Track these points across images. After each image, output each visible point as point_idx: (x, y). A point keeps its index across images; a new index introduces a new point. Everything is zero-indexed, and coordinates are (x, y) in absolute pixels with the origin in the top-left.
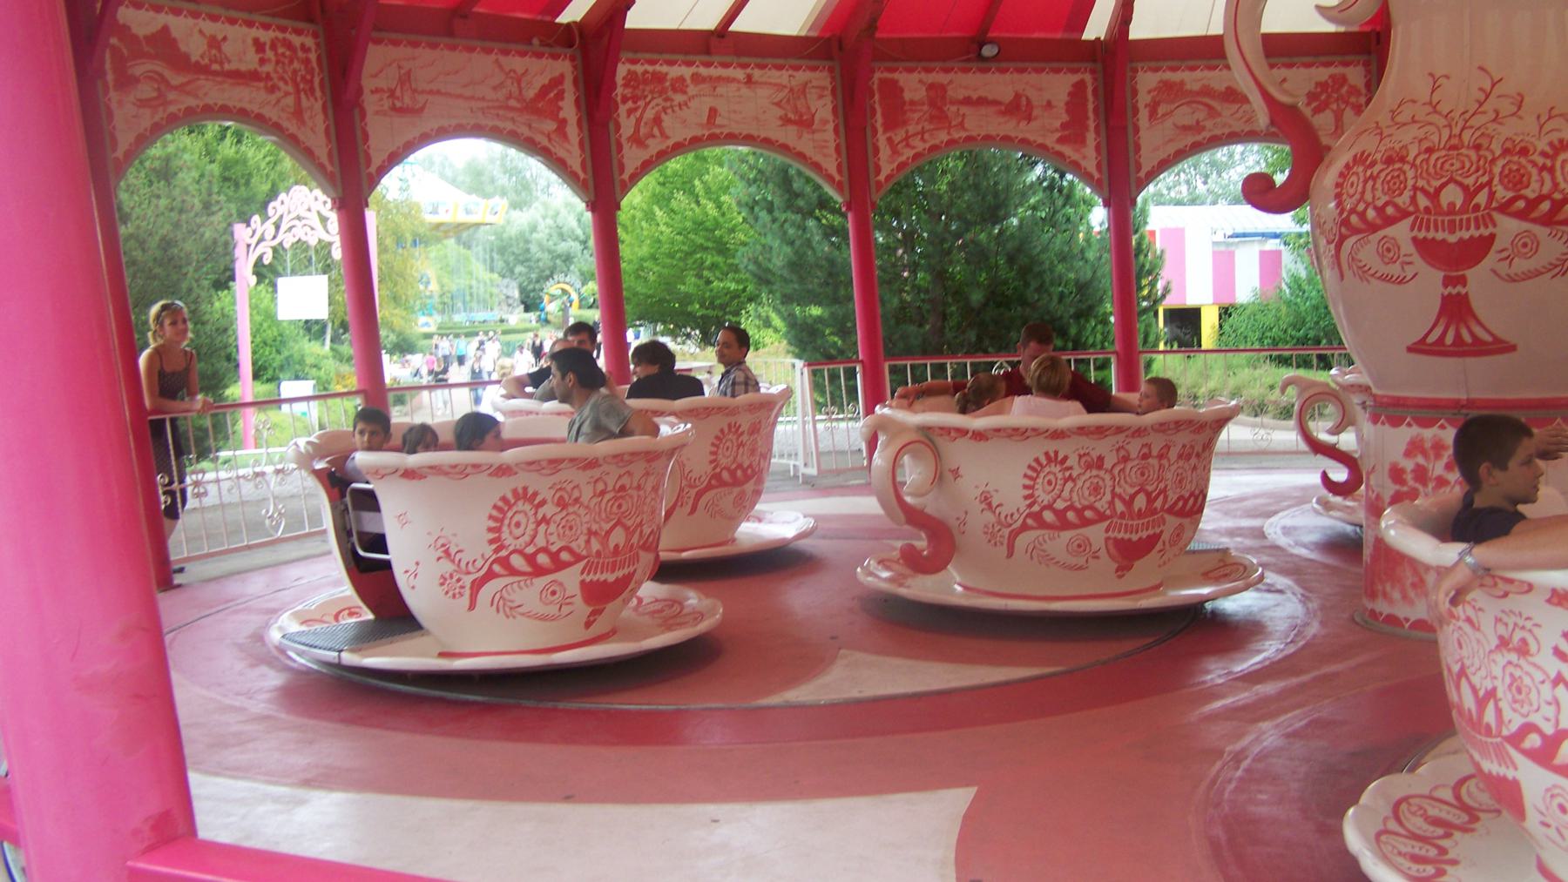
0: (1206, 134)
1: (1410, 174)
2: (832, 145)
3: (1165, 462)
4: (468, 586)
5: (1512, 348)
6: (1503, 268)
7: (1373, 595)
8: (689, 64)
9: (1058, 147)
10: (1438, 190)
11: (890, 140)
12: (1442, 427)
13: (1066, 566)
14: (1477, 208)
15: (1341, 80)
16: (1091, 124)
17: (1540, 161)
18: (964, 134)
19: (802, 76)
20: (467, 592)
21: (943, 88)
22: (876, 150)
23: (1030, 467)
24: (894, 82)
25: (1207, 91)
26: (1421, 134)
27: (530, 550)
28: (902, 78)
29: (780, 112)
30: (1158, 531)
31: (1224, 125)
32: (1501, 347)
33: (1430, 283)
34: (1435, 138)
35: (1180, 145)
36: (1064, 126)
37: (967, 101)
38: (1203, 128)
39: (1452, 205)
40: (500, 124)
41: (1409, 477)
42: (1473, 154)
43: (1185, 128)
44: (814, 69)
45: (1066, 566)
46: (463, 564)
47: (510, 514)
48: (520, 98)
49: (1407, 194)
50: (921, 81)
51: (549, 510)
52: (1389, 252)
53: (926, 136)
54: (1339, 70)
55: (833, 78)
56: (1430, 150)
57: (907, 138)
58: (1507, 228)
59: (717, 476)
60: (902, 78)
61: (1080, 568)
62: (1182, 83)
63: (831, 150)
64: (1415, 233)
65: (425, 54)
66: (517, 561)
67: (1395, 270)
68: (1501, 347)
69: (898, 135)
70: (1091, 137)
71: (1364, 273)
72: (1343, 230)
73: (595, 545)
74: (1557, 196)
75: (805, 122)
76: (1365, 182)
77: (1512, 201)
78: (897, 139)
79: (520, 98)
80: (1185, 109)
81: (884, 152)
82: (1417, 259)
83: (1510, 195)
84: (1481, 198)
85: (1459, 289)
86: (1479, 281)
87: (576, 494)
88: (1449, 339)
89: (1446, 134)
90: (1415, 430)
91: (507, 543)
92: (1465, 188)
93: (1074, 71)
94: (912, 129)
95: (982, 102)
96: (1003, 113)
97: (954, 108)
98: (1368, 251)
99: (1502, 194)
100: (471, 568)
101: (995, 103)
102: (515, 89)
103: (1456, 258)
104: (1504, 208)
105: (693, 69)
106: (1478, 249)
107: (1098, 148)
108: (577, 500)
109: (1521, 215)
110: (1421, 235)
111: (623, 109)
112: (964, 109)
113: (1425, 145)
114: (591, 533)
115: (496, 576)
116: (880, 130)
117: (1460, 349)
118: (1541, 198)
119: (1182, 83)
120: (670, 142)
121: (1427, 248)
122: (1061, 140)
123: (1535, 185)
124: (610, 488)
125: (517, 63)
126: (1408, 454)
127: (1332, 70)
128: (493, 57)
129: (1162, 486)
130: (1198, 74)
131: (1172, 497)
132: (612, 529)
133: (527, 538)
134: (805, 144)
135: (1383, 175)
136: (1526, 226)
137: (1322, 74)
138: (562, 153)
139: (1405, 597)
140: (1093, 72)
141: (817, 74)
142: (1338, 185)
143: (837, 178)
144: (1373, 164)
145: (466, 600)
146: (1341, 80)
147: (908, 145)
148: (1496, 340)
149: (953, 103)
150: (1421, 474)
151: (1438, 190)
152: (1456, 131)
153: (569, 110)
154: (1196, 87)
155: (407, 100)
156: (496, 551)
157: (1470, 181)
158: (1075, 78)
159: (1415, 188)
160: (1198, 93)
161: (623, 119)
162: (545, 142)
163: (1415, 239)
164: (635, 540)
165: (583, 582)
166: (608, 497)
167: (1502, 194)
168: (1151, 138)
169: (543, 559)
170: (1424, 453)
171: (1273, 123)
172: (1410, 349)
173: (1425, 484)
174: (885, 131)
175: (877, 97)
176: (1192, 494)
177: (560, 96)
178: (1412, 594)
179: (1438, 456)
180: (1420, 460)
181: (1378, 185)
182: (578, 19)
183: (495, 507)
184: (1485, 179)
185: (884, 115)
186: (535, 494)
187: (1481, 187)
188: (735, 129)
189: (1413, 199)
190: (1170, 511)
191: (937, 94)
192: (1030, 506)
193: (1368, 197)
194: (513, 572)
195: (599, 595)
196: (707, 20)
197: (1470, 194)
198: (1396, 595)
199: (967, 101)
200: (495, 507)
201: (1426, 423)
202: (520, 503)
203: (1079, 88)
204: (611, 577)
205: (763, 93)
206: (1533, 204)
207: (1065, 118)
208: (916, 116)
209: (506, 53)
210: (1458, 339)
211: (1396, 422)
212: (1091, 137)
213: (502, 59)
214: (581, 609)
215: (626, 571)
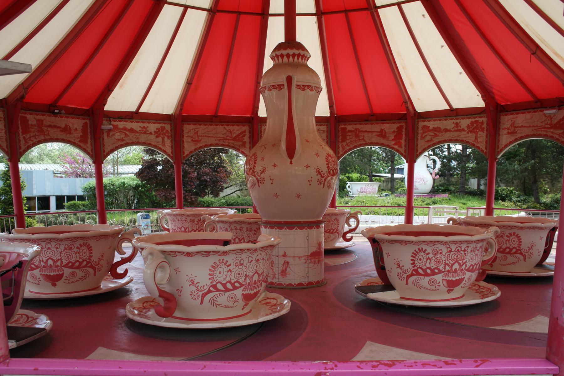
0: (125, 142)
2: (4, 138)
3: (466, 252)
4: (201, 295)
9: (79, 144)
11: (24, 138)
13: (225, 307)
15: (163, 128)
16: (89, 137)
18: (49, 137)
21: (42, 121)
22: (20, 141)
23: (413, 253)
24: (26, 118)
25: (125, 129)
27: (224, 282)
28: (28, 116)
30: (463, 277)
31: (130, 139)
35: (117, 145)
36: (81, 137)
37: (50, 126)
38: (124, 140)
40: (542, 133)
43: (119, 140)
46: (199, 288)
50: (34, 118)
51: (431, 256)
53: (37, 137)
54: (164, 125)
55: (4, 114)
57: (30, 138)
60: (28, 116)
61: (231, 307)
62: (117, 125)
63: (4, 140)
69: (28, 136)
70: (89, 141)
78: (27, 138)
80: (118, 134)
81: (22, 142)
87: (242, 262)
93: (84, 119)
94: (32, 134)
95: (55, 127)
96: (61, 131)
97: (46, 128)
101: (59, 127)
107: (91, 145)
108: (242, 264)
112: (49, 129)
114: (446, 264)
115: (211, 292)
116: (21, 134)
119: (117, 125)
122: (80, 141)
127: (161, 125)
129: (464, 261)
130: (122, 123)
131: (468, 265)
132: (254, 274)
137: (158, 126)
140: (89, 119)
143: (6, 150)
145: (199, 301)
146: (163, 128)
147: (30, 140)
149: (45, 126)
154: (122, 127)
155: (196, 138)
158: (85, 121)
160: (122, 129)
162: (557, 137)
164: (261, 279)
165: (243, 294)
168: (108, 142)
174: (23, 134)
175: (19, 122)
176: (475, 264)
185: (22, 129)
190: (468, 270)
191: (40, 123)
192: (414, 267)
194: (218, 290)
195: (248, 298)
196: (134, 109)
199: (50, 126)
202: (221, 265)
203: (85, 124)
204: (252, 292)
207: (81, 134)
208: (33, 130)
212: (89, 141)
214: (241, 303)
215: (257, 290)
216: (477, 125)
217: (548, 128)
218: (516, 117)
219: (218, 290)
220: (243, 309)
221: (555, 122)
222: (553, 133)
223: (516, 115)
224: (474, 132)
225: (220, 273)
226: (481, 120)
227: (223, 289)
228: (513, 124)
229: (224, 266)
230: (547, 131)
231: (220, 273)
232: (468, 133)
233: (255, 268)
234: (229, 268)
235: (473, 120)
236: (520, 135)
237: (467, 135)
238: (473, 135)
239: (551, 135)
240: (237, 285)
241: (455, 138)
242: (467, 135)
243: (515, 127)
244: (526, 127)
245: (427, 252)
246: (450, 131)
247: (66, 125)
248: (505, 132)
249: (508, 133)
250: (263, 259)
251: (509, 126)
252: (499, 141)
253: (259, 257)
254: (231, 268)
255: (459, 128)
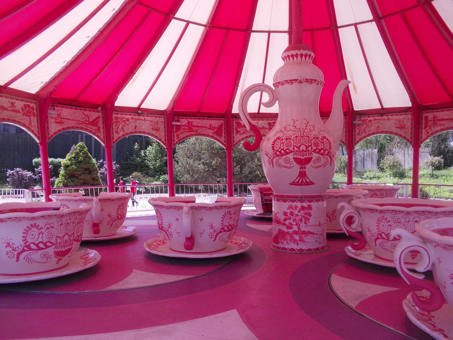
1: (293, 142)
4: (16, 254)
5: (314, 184)
6: (314, 165)
7: (278, 243)
8: (130, 115)
10: (300, 146)
12: (297, 202)
13: (40, 263)
14: (309, 150)
17: (321, 141)
19: (157, 119)
20: (16, 256)
26: (294, 133)
27: (37, 242)
29: (152, 127)
30: (71, 247)
32: (312, 183)
33: (297, 168)
34: (297, 134)
39: (303, 150)
40: (83, 127)
41: (288, 214)
42: (307, 138)
44: (160, 117)
45: (40, 263)
47: (29, 232)
48: (89, 122)
49: (292, 147)
52: (287, 161)
56: (296, 137)
58: (315, 155)
59: (118, 217)
64: (294, 156)
65: (65, 109)
66: (33, 246)
67: (288, 165)
68: (312, 183)
71: (280, 166)
72: (274, 155)
73: (59, 240)
74: (324, 149)
75: (157, 130)
76: (281, 144)
77: (316, 149)
79: (89, 122)
82: (294, 162)
83: (316, 148)
84: (310, 149)
85: (304, 170)
86: (309, 168)
87: (399, 220)
88: (300, 182)
89: (300, 133)
90: (290, 203)
91: (29, 241)
92: (306, 146)
98: (282, 161)
99: (314, 148)
100: (17, 249)
102: (87, 119)
103: (303, 162)
104: (314, 151)
105: (131, 116)
106: (308, 160)
108: (399, 222)
109: (317, 153)
110: (295, 157)
111: (114, 125)
113: (295, 135)
117: (302, 184)
118: (322, 149)
120: (125, 133)
121: (296, 160)
123: (320, 146)
124: (64, 223)
125: (87, 113)
126: (288, 209)
128: (82, 111)
132: (65, 235)
133: (36, 239)
134: (157, 134)
135: (285, 142)
136: (319, 155)
138: (99, 135)
139: (288, 243)
141: (161, 118)
142: (272, 144)
144: (282, 140)
145: (15, 259)
148: (311, 182)
150: (292, 214)
151: (300, 146)
152: (302, 133)
153: (101, 124)
156: (25, 243)
157: (307, 145)
159: (294, 146)
161: (114, 127)
162: (94, 132)
163: (294, 158)
165: (55, 252)
166: (63, 226)
167: (314, 148)
169: (41, 245)
170: (293, 209)
171: (251, 130)
172: (290, 184)
173: (293, 216)
177: (99, 121)
178: (289, 242)
179: (296, 209)
180: (292, 210)
181: (284, 145)
182: (34, 93)
183: (25, 230)
184: (310, 144)
186: (38, 226)
187: (310, 146)
188: (141, 130)
189: (294, 148)
193: (282, 147)
194: (31, 249)
195: (60, 254)
197: (307, 147)
198: (285, 242)
200: (25, 230)
201: (293, 201)
204: (64, 250)
205: (148, 122)
206: (320, 150)
209: (85, 110)
210: (302, 181)
211: (285, 201)
213: (84, 112)
214: (54, 259)
216: (29, 110)
217: (87, 124)
218: (62, 110)
219: (31, 249)
220: (57, 263)
221: (91, 120)
222: (91, 128)
223: (61, 108)
224: (28, 116)
225: (383, 226)
226: (31, 105)
227: (36, 248)
228: (59, 115)
229: (385, 222)
230: (86, 126)
231: (383, 226)
232: (23, 115)
233: (65, 230)
234: (389, 223)
235: (26, 103)
236: (67, 126)
237: (22, 117)
238: (27, 118)
239: (90, 129)
240: (48, 244)
241: (13, 119)
242: (22, 117)
243: (61, 118)
244: (70, 120)
245: (388, 220)
246: (6, 109)
247: (210, 125)
248: (53, 121)
249: (56, 122)
250: (73, 223)
251: (56, 116)
252: (48, 128)
253: (69, 221)
254: (43, 231)
255: (15, 109)
